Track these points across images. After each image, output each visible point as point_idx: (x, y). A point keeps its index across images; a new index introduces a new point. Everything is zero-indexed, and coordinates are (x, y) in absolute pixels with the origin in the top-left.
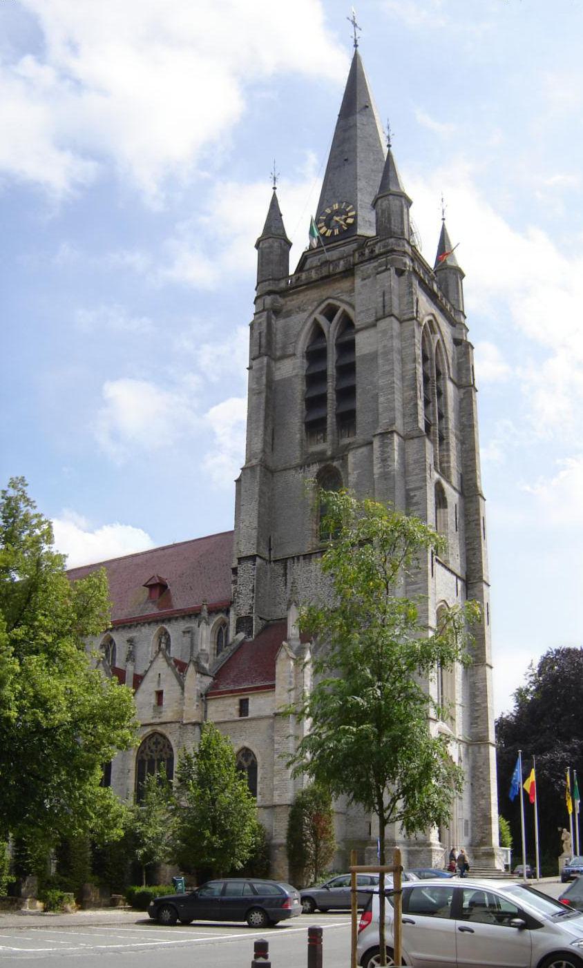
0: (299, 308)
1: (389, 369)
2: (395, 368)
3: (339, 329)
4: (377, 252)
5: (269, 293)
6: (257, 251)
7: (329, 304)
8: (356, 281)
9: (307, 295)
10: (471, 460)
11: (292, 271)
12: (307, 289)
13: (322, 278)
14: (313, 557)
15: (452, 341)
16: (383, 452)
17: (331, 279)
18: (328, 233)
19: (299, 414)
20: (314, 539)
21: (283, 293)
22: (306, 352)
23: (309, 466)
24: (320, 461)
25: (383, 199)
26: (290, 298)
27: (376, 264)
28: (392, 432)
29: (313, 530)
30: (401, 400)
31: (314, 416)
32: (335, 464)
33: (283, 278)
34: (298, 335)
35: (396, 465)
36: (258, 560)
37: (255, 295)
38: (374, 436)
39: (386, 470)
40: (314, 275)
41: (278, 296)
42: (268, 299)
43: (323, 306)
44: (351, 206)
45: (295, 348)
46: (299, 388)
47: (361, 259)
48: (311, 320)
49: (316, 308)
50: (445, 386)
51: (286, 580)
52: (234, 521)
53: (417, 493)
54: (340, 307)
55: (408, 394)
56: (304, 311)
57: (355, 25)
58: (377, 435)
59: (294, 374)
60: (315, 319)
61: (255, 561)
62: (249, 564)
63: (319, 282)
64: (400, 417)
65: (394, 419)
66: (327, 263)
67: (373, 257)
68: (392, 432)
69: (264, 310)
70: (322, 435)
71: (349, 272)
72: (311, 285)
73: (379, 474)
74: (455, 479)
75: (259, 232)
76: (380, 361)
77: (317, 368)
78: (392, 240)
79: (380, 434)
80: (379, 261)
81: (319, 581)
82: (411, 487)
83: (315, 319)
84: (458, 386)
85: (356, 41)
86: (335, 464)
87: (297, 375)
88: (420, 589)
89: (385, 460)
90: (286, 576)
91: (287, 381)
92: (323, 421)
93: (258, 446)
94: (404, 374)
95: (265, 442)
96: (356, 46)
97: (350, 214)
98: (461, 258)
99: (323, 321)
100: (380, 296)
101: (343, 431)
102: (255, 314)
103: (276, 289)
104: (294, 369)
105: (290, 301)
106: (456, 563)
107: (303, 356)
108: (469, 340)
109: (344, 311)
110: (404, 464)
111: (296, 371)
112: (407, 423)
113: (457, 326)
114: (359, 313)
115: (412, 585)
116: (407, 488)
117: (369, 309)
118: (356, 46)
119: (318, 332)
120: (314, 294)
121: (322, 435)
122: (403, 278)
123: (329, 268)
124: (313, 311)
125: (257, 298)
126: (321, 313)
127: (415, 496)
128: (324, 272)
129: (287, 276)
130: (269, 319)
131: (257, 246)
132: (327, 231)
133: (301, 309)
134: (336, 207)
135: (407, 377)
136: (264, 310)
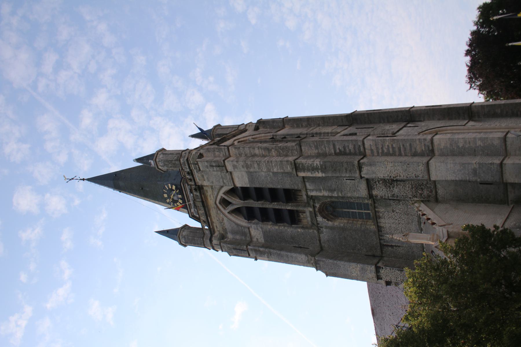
0: (221, 223)
1: (256, 164)
2: (256, 160)
3: (235, 198)
4: (188, 170)
5: (211, 241)
6: (188, 247)
7: (220, 203)
8: (205, 185)
9: (214, 217)
10: (329, 119)
11: (198, 225)
12: (210, 216)
13: (204, 206)
14: (379, 224)
15: (255, 131)
16: (308, 170)
17: (204, 200)
18: (180, 201)
19: (286, 228)
20: (368, 223)
21: (212, 231)
22: (248, 220)
23: (318, 224)
24: (316, 216)
25: (158, 165)
26: (215, 228)
27: (195, 171)
28: (295, 164)
29: (362, 224)
30: (277, 158)
31: (287, 217)
32: (317, 205)
33: (203, 231)
34: (238, 225)
35: (317, 162)
36: (380, 265)
37: (212, 250)
38: (297, 175)
39: (320, 168)
40: (202, 212)
41: (214, 235)
42: (215, 242)
43: (220, 207)
44: (166, 186)
45: (245, 227)
46: (269, 227)
47: (193, 181)
48: (230, 217)
49: (221, 212)
50: (281, 135)
51: (396, 246)
52: (354, 280)
53: (337, 147)
54: (222, 197)
55: (274, 153)
56: (223, 219)
57: (73, 179)
58: (296, 173)
59: (261, 229)
60: (228, 213)
61: (380, 267)
62: (382, 271)
63: (206, 209)
64: (286, 158)
65: (287, 161)
66: (194, 201)
67: (191, 173)
68: (295, 164)
69: (220, 245)
70: (300, 214)
71: (200, 188)
72: (207, 214)
73: (322, 174)
74: (339, 129)
75: (175, 243)
76: (252, 170)
77: (258, 213)
78: (181, 160)
79: (296, 171)
80: (193, 169)
81: (397, 221)
82: (333, 152)
83: (228, 213)
84: (283, 127)
85: (81, 179)
86: (317, 205)
87: (261, 228)
88: (403, 145)
89: (314, 169)
90: (393, 246)
91: (266, 234)
92: (291, 212)
93: (303, 257)
94: (261, 155)
95: (300, 253)
96: (83, 180)
97: (170, 187)
98: (208, 126)
99: (230, 208)
100: (213, 168)
101: (298, 200)
102: (222, 251)
103: (209, 235)
104: (258, 229)
105: (217, 228)
106: (395, 127)
107: (250, 223)
108: (255, 122)
109: (224, 193)
110: (318, 156)
111: (259, 228)
112: (292, 154)
113: (247, 128)
114: (224, 183)
115: (401, 152)
116: (334, 154)
117: (222, 176)
118: (83, 180)
119: (237, 211)
120: (213, 212)
121: (300, 214)
122: (204, 155)
123: (198, 201)
124: (223, 214)
125: (214, 249)
126: (225, 209)
127: (339, 148)
128: (199, 204)
129: (202, 229)
130: (225, 243)
131: (185, 246)
132: (179, 202)
133: (222, 222)
134: (166, 196)
135: (264, 153)
136: (220, 245)
